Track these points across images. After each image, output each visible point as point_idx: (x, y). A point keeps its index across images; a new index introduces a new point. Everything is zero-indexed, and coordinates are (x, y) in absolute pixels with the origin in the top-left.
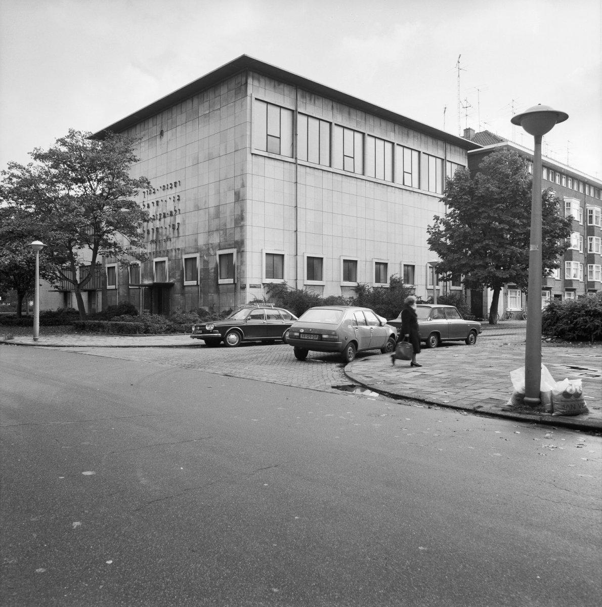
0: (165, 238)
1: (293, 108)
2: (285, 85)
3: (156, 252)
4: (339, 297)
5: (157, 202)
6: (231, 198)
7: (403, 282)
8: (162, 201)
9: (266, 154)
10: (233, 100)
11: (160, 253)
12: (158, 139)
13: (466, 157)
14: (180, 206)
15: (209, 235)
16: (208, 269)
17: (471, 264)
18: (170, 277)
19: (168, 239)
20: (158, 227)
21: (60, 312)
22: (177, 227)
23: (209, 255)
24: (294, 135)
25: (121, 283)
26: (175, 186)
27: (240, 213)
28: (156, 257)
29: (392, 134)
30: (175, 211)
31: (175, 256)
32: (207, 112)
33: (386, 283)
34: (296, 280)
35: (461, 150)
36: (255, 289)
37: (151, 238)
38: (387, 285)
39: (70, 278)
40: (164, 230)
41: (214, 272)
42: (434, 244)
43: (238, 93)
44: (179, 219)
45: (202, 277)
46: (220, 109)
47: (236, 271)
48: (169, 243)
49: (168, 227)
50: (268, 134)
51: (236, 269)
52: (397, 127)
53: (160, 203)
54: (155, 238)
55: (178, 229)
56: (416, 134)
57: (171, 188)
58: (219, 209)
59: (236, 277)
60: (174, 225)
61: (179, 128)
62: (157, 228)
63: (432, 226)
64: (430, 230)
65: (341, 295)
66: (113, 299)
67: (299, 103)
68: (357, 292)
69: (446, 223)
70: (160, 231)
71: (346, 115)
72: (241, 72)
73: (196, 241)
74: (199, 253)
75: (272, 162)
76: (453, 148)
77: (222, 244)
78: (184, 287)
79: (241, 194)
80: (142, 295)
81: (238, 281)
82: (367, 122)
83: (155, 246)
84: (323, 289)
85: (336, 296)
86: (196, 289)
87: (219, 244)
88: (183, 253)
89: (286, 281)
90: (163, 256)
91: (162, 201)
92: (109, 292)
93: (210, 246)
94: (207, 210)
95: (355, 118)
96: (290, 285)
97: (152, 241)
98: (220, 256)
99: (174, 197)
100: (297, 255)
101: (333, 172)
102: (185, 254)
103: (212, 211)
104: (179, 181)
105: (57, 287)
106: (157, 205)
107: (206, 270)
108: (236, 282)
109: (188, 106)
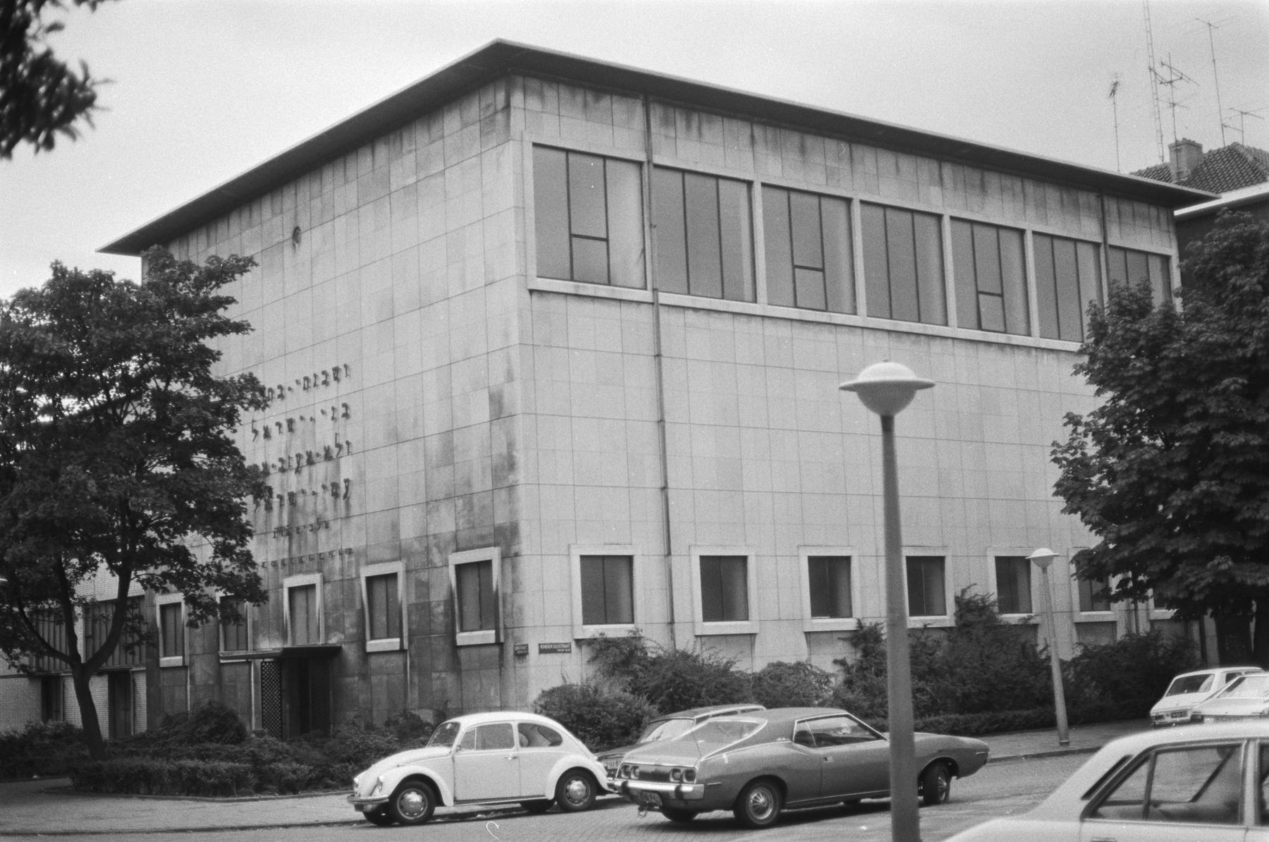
0: (312, 520)
1: (642, 157)
2: (615, 98)
3: (291, 559)
4: (799, 664)
5: (290, 422)
6: (482, 411)
7: (996, 609)
8: (302, 418)
9: (568, 287)
10: (476, 149)
11: (301, 562)
12: (288, 251)
13: (1171, 229)
14: (351, 432)
15: (428, 512)
16: (429, 603)
17: (1169, 550)
18: (328, 630)
19: (322, 524)
20: (294, 490)
21: (34, 733)
22: (343, 491)
23: (429, 565)
24: (647, 228)
25: (199, 650)
26: (336, 379)
27: (504, 451)
28: (290, 575)
29: (935, 191)
30: (339, 446)
31: (342, 570)
32: (412, 180)
33: (945, 614)
34: (672, 623)
35: (1153, 211)
36: (554, 655)
37: (275, 523)
38: (948, 619)
39: (58, 648)
40: (310, 499)
41: (445, 614)
42: (1074, 490)
43: (488, 133)
44: (347, 469)
45: (414, 627)
46: (443, 173)
47: (501, 609)
48: (322, 534)
49: (319, 490)
51: (501, 603)
52: (948, 170)
53: (298, 425)
54: (285, 524)
55: (345, 496)
56: (1007, 182)
57: (325, 383)
58: (451, 442)
59: (501, 625)
60: (335, 486)
61: (340, 223)
62: (292, 495)
63: (1064, 441)
64: (1059, 455)
65: (803, 659)
66: (178, 694)
67: (655, 139)
68: (855, 645)
69: (1099, 435)
70: (300, 500)
71: (793, 156)
72: (503, 70)
73: (395, 527)
74: (404, 560)
75: (588, 307)
76: (1126, 208)
77: (463, 535)
78: (366, 656)
79: (506, 400)
80: (256, 682)
81: (506, 637)
82: (859, 168)
83: (287, 544)
84: (752, 645)
85: (790, 660)
86: (397, 660)
87: (456, 536)
88: (362, 561)
89: (640, 626)
90: (308, 572)
91: (302, 418)
92: (165, 675)
93: (432, 541)
94: (420, 443)
95: (818, 159)
96: (655, 641)
97: (280, 530)
98: (459, 568)
99: (333, 409)
100: (669, 554)
101: (763, 317)
102: (368, 564)
103: (434, 445)
104: (346, 366)
105: (23, 667)
106: (291, 430)
107: (423, 608)
108: (502, 640)
109: (364, 165)
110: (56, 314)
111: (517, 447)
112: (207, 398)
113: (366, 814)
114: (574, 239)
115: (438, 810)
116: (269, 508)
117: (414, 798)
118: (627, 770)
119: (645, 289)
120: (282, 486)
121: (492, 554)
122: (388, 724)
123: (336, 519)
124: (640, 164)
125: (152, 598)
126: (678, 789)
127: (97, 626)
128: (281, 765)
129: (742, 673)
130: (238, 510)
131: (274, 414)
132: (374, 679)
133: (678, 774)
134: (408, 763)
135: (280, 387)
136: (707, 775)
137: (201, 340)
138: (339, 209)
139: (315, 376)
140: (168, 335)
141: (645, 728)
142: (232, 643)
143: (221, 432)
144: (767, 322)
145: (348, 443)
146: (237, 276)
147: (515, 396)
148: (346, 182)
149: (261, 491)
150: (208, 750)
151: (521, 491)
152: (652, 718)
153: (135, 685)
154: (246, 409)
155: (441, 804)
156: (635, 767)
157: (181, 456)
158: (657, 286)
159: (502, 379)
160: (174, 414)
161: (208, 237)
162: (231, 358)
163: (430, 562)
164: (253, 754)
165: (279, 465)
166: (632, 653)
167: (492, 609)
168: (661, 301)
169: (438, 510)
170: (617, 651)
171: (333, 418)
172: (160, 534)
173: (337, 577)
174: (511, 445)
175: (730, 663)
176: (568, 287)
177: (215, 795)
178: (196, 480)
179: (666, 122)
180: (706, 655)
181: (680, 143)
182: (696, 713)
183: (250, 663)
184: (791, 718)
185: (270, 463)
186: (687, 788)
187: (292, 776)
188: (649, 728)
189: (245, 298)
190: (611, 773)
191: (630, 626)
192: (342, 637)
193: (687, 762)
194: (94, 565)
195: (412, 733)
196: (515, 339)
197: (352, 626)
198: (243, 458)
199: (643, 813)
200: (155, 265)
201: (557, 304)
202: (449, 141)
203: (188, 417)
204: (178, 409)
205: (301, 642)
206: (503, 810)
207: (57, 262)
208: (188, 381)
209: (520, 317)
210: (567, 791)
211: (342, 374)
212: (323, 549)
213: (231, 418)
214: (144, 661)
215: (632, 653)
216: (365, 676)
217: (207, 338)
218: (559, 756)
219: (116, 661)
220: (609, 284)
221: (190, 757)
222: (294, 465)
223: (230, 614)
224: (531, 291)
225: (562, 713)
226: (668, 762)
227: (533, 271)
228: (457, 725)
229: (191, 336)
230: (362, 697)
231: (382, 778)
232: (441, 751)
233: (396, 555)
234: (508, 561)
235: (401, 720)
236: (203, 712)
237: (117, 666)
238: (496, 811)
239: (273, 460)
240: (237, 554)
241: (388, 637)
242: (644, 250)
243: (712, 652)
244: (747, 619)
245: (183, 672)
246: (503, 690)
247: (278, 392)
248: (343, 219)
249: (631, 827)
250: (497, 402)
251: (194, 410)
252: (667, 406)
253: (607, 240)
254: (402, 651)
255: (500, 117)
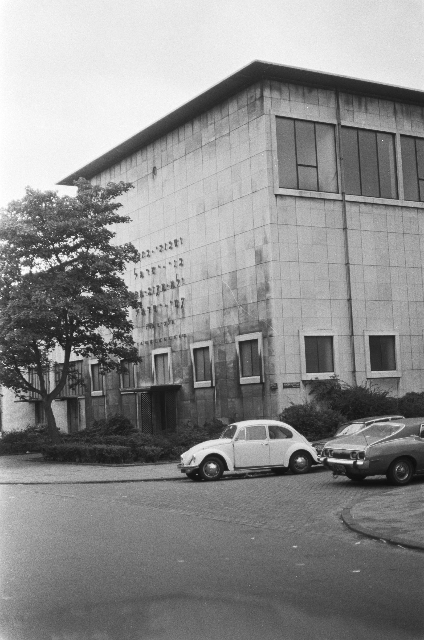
0: (165, 320)
1: (335, 122)
2: (320, 90)
3: (155, 340)
6: (251, 260)
8: (159, 267)
9: (296, 193)
10: (246, 120)
11: (160, 341)
14: (184, 273)
15: (224, 315)
16: (226, 362)
18: (175, 377)
19: (170, 322)
20: (156, 304)
21: (31, 430)
22: (180, 304)
23: (225, 342)
24: (338, 160)
26: (176, 246)
27: (263, 281)
28: (155, 348)
30: (178, 281)
31: (181, 345)
32: (213, 139)
36: (291, 389)
37: (147, 322)
40: (164, 309)
43: (252, 111)
44: (183, 293)
45: (218, 375)
46: (229, 134)
48: (171, 327)
49: (169, 304)
50: (420, 177)
53: (157, 270)
54: (152, 321)
55: (182, 307)
57: (171, 248)
59: (263, 374)
60: (176, 301)
61: (176, 163)
62: (155, 307)
67: (342, 112)
70: (159, 310)
73: (207, 322)
78: (194, 390)
80: (139, 404)
81: (266, 380)
83: (153, 332)
84: (398, 383)
86: (209, 393)
87: (239, 327)
88: (191, 341)
90: (164, 347)
91: (159, 267)
92: (94, 400)
93: (227, 330)
94: (220, 278)
97: (149, 325)
98: (241, 343)
99: (175, 261)
100: (352, 335)
101: (402, 207)
103: (226, 279)
104: (181, 239)
105: (23, 397)
106: (154, 273)
107: (222, 365)
108: (264, 381)
110: (30, 213)
111: (270, 279)
112: (107, 256)
113: (187, 474)
114: (299, 168)
115: (225, 473)
116: (143, 314)
117: (213, 466)
118: (327, 453)
119: (338, 193)
120: (150, 303)
121: (258, 336)
122: (205, 425)
123: (177, 319)
124: (333, 126)
125: (87, 361)
126: (355, 463)
127: (34, 375)
128: (146, 448)
129: (392, 398)
130: (124, 315)
131: (144, 265)
132: (198, 402)
133: (355, 455)
134: (209, 447)
135: (148, 251)
136: (371, 456)
137: (104, 226)
138: (176, 156)
139: (165, 244)
140: (87, 222)
141: (339, 428)
142: (127, 384)
143: (115, 274)
144: (404, 210)
145: (183, 279)
146: (123, 192)
147: (269, 252)
148: (179, 142)
149: (135, 305)
150: (110, 439)
151: (273, 303)
152: (343, 422)
153: (80, 405)
154: (128, 262)
155: (227, 469)
156: (331, 451)
157: (96, 287)
158: (344, 191)
159: (261, 243)
160: (91, 265)
161: (110, 174)
162: (120, 236)
163: (225, 340)
164: (132, 441)
165: (148, 291)
166: (332, 388)
167: (258, 365)
168: (346, 199)
169: (229, 313)
170: (324, 387)
171: (175, 266)
172: (86, 328)
173: (179, 349)
174: (267, 278)
175: (386, 393)
176: (296, 193)
177: (112, 463)
178: (102, 299)
179: (348, 103)
180: (373, 389)
181: (356, 114)
182: (367, 420)
183: (135, 394)
184: (418, 424)
185: (144, 290)
186: (360, 463)
187: (151, 453)
188: (341, 428)
189: (127, 204)
190: (319, 453)
191: (332, 374)
192: (182, 380)
193: (360, 448)
194: (54, 345)
195: (215, 431)
196: (268, 221)
197: (186, 374)
198: (127, 287)
199: (335, 476)
200: (82, 189)
201: (290, 201)
202: (231, 117)
203: (98, 266)
204: (94, 262)
205: (161, 383)
206: (261, 473)
207: (28, 187)
208: (97, 248)
209: (271, 209)
210: (296, 462)
211: (179, 243)
212: (171, 334)
213: (121, 267)
214: (84, 394)
215: (332, 388)
216: (193, 401)
217: (108, 224)
218: (293, 443)
219: (69, 393)
220: (318, 191)
221: (101, 443)
222: (156, 291)
223: (122, 370)
224: (276, 195)
225: (294, 420)
226: (349, 448)
227: (277, 184)
228: (235, 427)
229: (99, 224)
230: (192, 411)
231: (195, 456)
232: (227, 441)
233: (209, 337)
234: (266, 339)
235: (212, 423)
236: (113, 419)
237: (71, 396)
238: (258, 473)
239: (145, 289)
240: (125, 337)
241: (205, 380)
242: (337, 172)
243: (376, 387)
244: (395, 369)
245: (103, 399)
246: (265, 408)
247: (147, 253)
248: (178, 161)
249: (330, 484)
250: (259, 254)
251: (101, 263)
252: (350, 256)
253: (317, 167)
254: (212, 387)
255: (258, 103)
